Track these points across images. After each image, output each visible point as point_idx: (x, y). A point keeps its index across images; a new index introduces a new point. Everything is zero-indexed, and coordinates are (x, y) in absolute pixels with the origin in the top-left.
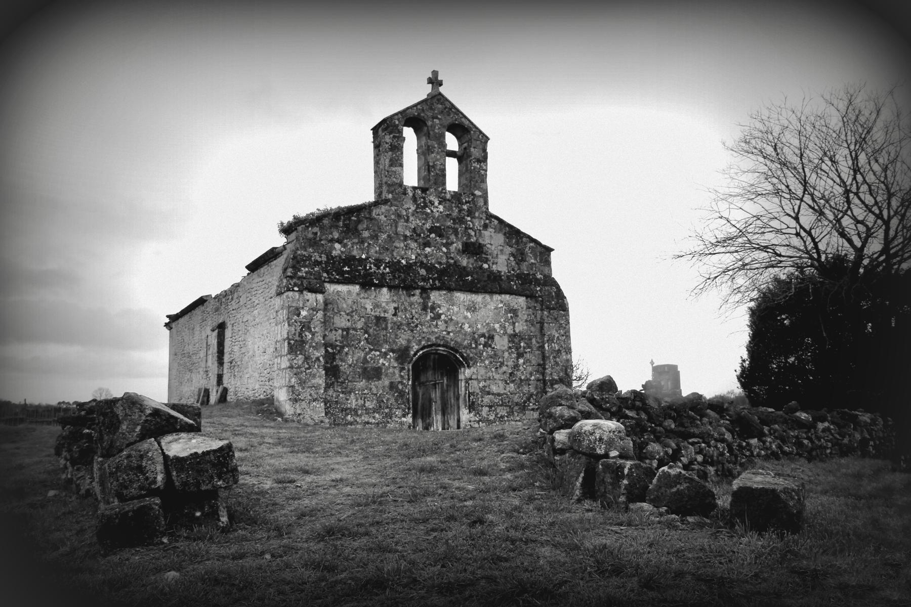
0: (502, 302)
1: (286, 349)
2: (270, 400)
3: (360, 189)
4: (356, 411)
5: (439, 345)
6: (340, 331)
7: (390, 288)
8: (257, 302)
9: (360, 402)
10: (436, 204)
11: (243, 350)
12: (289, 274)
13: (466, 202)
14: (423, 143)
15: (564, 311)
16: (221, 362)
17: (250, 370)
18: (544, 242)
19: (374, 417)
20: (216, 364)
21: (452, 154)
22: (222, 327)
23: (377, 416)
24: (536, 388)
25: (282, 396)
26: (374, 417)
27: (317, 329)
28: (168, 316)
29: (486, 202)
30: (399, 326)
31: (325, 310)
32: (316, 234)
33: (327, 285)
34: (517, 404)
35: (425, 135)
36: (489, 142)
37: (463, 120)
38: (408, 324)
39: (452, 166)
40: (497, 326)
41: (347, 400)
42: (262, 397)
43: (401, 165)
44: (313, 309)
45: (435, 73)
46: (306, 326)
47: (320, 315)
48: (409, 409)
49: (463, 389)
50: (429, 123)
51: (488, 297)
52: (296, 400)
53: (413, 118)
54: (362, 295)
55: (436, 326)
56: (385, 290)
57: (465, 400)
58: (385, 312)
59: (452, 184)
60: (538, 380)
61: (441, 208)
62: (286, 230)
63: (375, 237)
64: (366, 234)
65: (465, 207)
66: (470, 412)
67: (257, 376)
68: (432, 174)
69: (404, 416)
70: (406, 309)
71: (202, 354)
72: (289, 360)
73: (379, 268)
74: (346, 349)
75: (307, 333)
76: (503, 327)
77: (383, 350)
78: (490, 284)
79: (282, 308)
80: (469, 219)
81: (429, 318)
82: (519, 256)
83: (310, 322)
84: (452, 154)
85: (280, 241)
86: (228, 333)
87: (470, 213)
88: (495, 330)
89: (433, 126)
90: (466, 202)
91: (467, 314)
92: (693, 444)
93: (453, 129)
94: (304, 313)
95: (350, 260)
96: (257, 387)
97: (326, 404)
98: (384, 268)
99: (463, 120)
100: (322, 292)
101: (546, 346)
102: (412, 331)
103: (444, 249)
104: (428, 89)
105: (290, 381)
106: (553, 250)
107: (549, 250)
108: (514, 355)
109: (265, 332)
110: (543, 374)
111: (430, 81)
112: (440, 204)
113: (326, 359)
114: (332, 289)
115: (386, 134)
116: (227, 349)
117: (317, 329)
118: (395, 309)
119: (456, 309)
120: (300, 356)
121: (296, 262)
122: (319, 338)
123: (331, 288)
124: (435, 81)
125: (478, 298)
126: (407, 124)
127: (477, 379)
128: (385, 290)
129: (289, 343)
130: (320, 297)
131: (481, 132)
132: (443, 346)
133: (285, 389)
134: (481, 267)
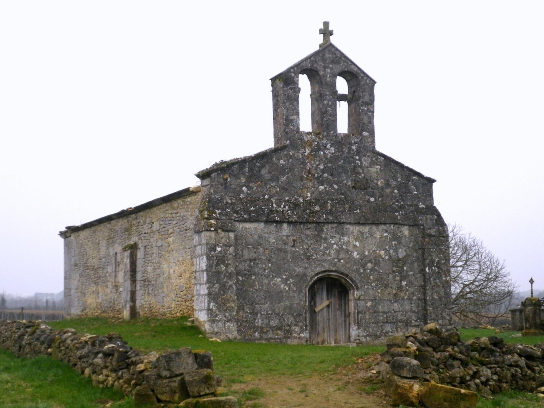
0: (386, 231)
1: (205, 279)
3: (262, 139)
4: (262, 328)
5: (332, 271)
6: (248, 262)
8: (171, 231)
9: (266, 321)
11: (158, 271)
12: (206, 216)
13: (355, 143)
14: (317, 89)
16: (133, 280)
17: (165, 290)
18: (426, 174)
19: (277, 334)
21: (343, 98)
22: (133, 248)
23: (280, 332)
24: (418, 307)
26: (277, 334)
29: (373, 142)
30: (295, 257)
31: (236, 245)
32: (226, 179)
33: (237, 224)
35: (318, 82)
36: (376, 86)
38: (305, 254)
39: (342, 109)
40: (382, 252)
41: (255, 319)
42: (178, 314)
43: (298, 114)
44: (225, 245)
45: (326, 24)
47: (232, 249)
48: (306, 326)
49: (353, 308)
50: (321, 73)
51: (374, 228)
53: (309, 67)
54: (266, 230)
55: (329, 254)
56: (285, 226)
57: (354, 317)
58: (285, 244)
59: (342, 126)
60: (419, 299)
61: (333, 150)
62: (203, 175)
64: (267, 177)
66: (359, 328)
67: (174, 296)
68: (324, 118)
69: (302, 332)
70: (303, 241)
71: (110, 269)
72: (208, 288)
73: (280, 206)
74: (253, 277)
75: (222, 266)
77: (284, 277)
80: (357, 157)
81: (322, 247)
82: (404, 188)
84: (343, 98)
85: (195, 183)
86: (140, 254)
87: (358, 152)
88: (381, 256)
89: (324, 76)
90: (355, 143)
91: (354, 245)
92: (490, 368)
93: (343, 74)
94: (219, 249)
98: (284, 206)
99: (353, 66)
101: (427, 269)
102: (308, 259)
106: (434, 181)
107: (431, 181)
108: (398, 278)
109: (181, 259)
110: (425, 294)
111: (322, 32)
112: (331, 146)
113: (229, 279)
116: (139, 268)
118: (294, 241)
119: (346, 239)
120: (217, 285)
121: (211, 204)
122: (231, 269)
123: (240, 226)
124: (326, 32)
126: (302, 73)
128: (285, 226)
130: (232, 235)
131: (368, 76)
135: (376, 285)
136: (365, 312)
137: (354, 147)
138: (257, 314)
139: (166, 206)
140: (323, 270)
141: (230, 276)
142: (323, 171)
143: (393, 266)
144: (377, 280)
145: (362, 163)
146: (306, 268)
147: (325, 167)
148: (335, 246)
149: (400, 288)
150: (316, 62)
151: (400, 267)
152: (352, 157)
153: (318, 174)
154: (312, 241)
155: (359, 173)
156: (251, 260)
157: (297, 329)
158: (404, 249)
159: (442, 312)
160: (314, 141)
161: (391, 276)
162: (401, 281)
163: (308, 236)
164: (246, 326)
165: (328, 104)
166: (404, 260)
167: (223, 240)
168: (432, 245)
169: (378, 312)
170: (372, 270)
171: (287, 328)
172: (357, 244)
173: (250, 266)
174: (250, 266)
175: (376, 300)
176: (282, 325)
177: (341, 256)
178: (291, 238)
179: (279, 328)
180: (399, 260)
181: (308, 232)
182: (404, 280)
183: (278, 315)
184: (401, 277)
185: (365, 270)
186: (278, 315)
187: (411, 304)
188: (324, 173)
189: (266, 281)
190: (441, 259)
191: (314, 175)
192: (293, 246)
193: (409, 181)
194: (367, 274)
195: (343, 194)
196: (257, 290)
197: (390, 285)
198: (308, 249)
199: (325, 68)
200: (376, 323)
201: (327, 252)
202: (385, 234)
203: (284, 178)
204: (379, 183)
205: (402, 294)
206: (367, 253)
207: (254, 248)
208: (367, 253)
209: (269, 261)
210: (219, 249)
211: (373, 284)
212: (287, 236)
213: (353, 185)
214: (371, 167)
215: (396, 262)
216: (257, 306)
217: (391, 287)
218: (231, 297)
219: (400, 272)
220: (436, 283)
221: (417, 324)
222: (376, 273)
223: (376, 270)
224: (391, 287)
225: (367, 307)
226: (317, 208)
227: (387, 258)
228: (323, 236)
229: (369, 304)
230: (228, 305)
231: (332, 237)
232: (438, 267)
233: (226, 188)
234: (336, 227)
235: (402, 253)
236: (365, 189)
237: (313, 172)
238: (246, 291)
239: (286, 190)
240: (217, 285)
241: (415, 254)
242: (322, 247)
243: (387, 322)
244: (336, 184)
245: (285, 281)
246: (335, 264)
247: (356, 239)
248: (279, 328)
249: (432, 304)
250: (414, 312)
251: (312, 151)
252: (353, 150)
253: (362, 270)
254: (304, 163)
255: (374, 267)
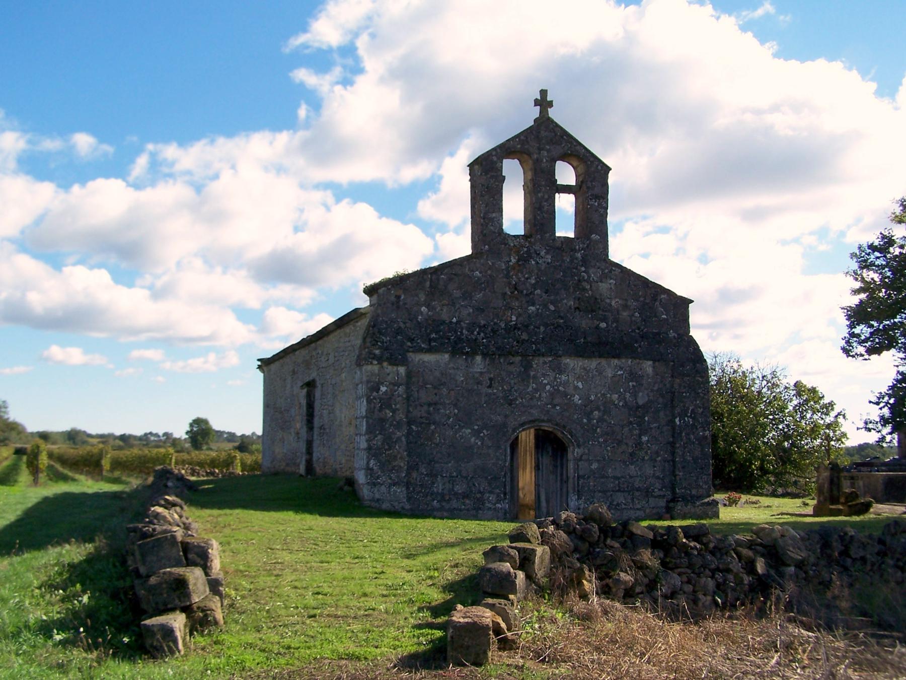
0: (621, 369)
2: (351, 482)
4: (443, 495)
5: (543, 421)
6: (426, 407)
7: (485, 355)
10: (543, 253)
15: (702, 377)
19: (464, 504)
20: (305, 429)
23: (468, 502)
25: (361, 478)
26: (464, 504)
27: (398, 406)
28: (259, 360)
31: (408, 385)
34: (638, 490)
36: (610, 174)
37: (578, 147)
41: (433, 483)
44: (394, 384)
45: (544, 93)
46: (387, 402)
47: (401, 389)
48: (505, 494)
51: (604, 362)
52: (374, 485)
54: (452, 365)
55: (539, 398)
56: (479, 358)
59: (565, 229)
60: (665, 461)
61: (549, 258)
62: (370, 291)
63: (467, 296)
64: (457, 293)
65: (579, 255)
68: (540, 213)
69: (498, 501)
70: (503, 379)
74: (433, 427)
75: (388, 411)
76: (621, 397)
77: (476, 427)
78: (602, 347)
79: (361, 382)
80: (583, 269)
81: (530, 389)
83: (390, 398)
87: (585, 262)
94: (383, 389)
95: (436, 324)
96: (343, 461)
97: (408, 488)
98: (479, 334)
99: (578, 147)
100: (404, 362)
101: (677, 420)
102: (510, 404)
103: (552, 308)
104: (536, 112)
105: (368, 463)
106: (692, 301)
110: (673, 453)
111: (537, 103)
112: (547, 253)
114: (417, 360)
115: (485, 176)
116: (316, 413)
117: (398, 406)
118: (491, 379)
119: (564, 377)
120: (379, 437)
122: (401, 416)
124: (543, 102)
125: (593, 364)
127: (588, 460)
128: (479, 358)
129: (367, 422)
130: (402, 370)
132: (549, 421)
133: (363, 471)
134: (597, 327)
135: (605, 441)
136: (589, 477)
137: (579, 255)
138: (436, 476)
139: (303, 352)
140: (531, 418)
141: (398, 426)
142: (534, 287)
143: (630, 415)
144: (607, 434)
145: (589, 277)
146: (506, 416)
147: (537, 282)
148: (548, 387)
149: (639, 444)
150: (528, 142)
151: (639, 417)
152: (576, 269)
153: (527, 290)
154: (516, 381)
155: (584, 289)
156: (430, 405)
157: (492, 498)
158: (646, 392)
159: (698, 478)
160: (522, 246)
161: (626, 429)
162: (640, 436)
163: (511, 373)
164: (421, 492)
165: (543, 197)
166: (645, 407)
167: (389, 378)
168: (685, 387)
169: (607, 477)
170: (601, 420)
171: (479, 496)
172: (580, 385)
173: (429, 413)
174: (429, 413)
175: (604, 459)
176: (471, 491)
177: (556, 401)
178: (486, 377)
179: (465, 496)
180: (638, 407)
181: (511, 368)
182: (645, 434)
183: (466, 478)
184: (640, 430)
185: (589, 420)
186: (466, 478)
187: (654, 467)
188: (535, 289)
189: (450, 433)
190: (697, 406)
191: (522, 292)
192: (490, 386)
193: (656, 300)
194: (593, 425)
195: (562, 318)
196: (437, 445)
197: (625, 441)
198: (510, 391)
199: (540, 149)
200: (604, 492)
201: (537, 395)
202: (619, 373)
203: (479, 296)
204: (613, 303)
205: (642, 453)
206: (593, 398)
207: (435, 388)
208: (593, 398)
209: (455, 405)
210: (383, 389)
211: (601, 440)
212: (481, 373)
213: (577, 305)
214: (601, 282)
215: (636, 410)
216: (437, 465)
217: (627, 444)
218: (399, 452)
219: (639, 424)
220: (690, 439)
221: (662, 493)
222: (605, 424)
223: (606, 421)
224: (627, 444)
225: (591, 470)
226: (525, 336)
227: (621, 404)
228: (532, 373)
229: (595, 466)
230: (396, 463)
231: (544, 375)
232: (693, 419)
233: (398, 307)
234: (550, 361)
235: (642, 399)
236: (593, 311)
237: (520, 288)
238: (422, 444)
239: (483, 311)
240: (379, 437)
241: (661, 400)
242: (530, 389)
243: (619, 491)
244: (552, 303)
245: (476, 433)
246: (548, 411)
247: (579, 378)
248: (465, 496)
249: (683, 467)
250: (658, 478)
251: (519, 260)
252: (577, 259)
253: (585, 420)
254: (507, 276)
255: (604, 415)
